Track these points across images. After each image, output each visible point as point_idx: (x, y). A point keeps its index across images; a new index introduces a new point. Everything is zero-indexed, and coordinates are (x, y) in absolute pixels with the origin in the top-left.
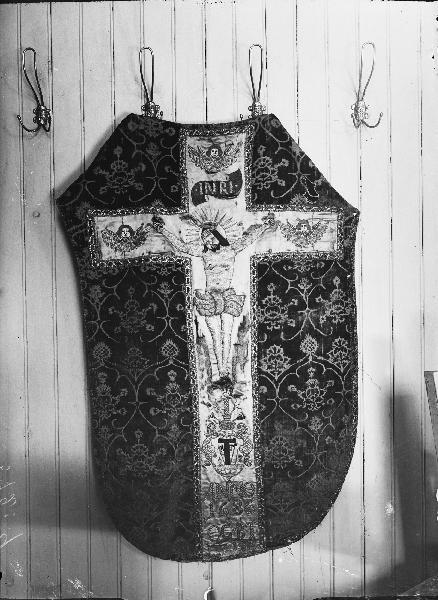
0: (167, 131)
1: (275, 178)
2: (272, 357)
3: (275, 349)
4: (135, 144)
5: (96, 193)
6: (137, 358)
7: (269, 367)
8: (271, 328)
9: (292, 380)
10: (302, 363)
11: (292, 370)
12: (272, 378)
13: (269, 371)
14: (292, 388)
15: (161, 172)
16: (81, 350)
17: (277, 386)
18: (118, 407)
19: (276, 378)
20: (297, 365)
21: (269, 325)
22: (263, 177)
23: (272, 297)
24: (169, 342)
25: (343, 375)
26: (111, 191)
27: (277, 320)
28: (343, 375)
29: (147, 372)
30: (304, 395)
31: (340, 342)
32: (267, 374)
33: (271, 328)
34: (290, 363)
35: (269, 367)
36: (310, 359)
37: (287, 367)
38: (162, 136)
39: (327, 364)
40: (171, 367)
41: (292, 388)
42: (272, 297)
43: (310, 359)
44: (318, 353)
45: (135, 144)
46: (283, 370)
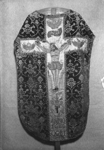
3: (71, 79)
5: (41, 34)
8: (27, 33)
11: (76, 85)
12: (70, 88)
13: (69, 86)
14: (76, 90)
32: (69, 86)
33: (27, 33)
35: (70, 84)
37: (75, 84)
40: (40, 84)
46: (73, 85)
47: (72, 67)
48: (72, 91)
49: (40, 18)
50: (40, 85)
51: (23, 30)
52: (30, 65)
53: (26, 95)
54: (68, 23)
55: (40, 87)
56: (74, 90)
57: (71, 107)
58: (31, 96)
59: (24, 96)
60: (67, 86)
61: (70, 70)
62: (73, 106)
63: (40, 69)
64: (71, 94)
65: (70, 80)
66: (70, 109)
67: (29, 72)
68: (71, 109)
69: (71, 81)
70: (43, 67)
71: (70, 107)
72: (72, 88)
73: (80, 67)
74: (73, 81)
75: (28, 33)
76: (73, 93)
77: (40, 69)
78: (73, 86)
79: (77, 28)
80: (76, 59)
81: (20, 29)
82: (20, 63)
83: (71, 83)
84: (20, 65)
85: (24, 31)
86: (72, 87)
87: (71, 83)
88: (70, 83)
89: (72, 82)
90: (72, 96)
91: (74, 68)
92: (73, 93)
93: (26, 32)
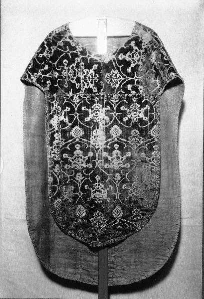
2: (111, 80)
5: (121, 120)
6: (137, 137)
7: (117, 83)
8: (97, 79)
9: (124, 70)
11: (118, 69)
12: (123, 81)
13: (119, 83)
14: (129, 71)
15: (79, 110)
16: (156, 286)
17: (128, 79)
19: (123, 79)
20: (116, 66)
24: (115, 127)
26: (130, 120)
27: (92, 76)
31: (137, 211)
32: (120, 85)
33: (97, 79)
35: (117, 83)
36: (118, 221)
37: (116, 71)
40: (78, 143)
43: (118, 221)
46: (119, 75)
48: (130, 79)
49: (124, 168)
50: (78, 145)
51: (89, 88)
53: (66, 83)
56: (128, 75)
59: (66, 80)
60: (175, 72)
61: (92, 81)
62: (98, 105)
63: (80, 192)
65: (108, 81)
68: (133, 110)
69: (111, 80)
70: (86, 187)
72: (123, 77)
74: (110, 74)
75: (98, 78)
77: (80, 192)
78: (120, 77)
81: (141, 23)
83: (114, 79)
85: (91, 86)
86: (123, 79)
87: (114, 79)
88: (113, 81)
89: (113, 77)
93: (95, 82)
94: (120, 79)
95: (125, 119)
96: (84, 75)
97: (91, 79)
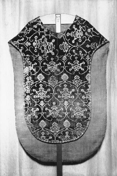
0: (36, 49)
1: (51, 43)
2: (63, 48)
3: (61, 47)
4: (30, 38)
9: (70, 42)
10: (65, 38)
11: (67, 41)
12: (70, 48)
13: (68, 49)
14: (73, 42)
18: (71, 95)
19: (70, 47)
21: (53, 116)
22: (50, 47)
23: (52, 62)
25: (72, 46)
27: (51, 46)
28: (72, 46)
29: (81, 85)
30: (76, 37)
34: (64, 42)
35: (66, 49)
37: (66, 43)
38: (34, 47)
39: (72, 84)
41: (73, 42)
42: (52, 62)
44: (69, 80)
45: (30, 38)
46: (67, 45)
47: (48, 46)
48: (74, 46)
50: (65, 85)
52: (76, 62)
54: (90, 46)
55: (67, 134)
57: (52, 108)
58: (80, 46)
61: (51, 49)
64: (78, 47)
66: (52, 110)
67: (75, 69)
71: (52, 108)
73: (50, 36)
74: (62, 45)
76: (40, 33)
78: (68, 46)
79: (79, 48)
80: (29, 39)
82: (65, 104)
84: (65, 106)
86: (70, 47)
88: (64, 48)
90: (36, 32)
91: (49, 44)
92: (40, 33)
94: (68, 47)
95: (70, 70)
96: (47, 45)
97: (76, 67)
